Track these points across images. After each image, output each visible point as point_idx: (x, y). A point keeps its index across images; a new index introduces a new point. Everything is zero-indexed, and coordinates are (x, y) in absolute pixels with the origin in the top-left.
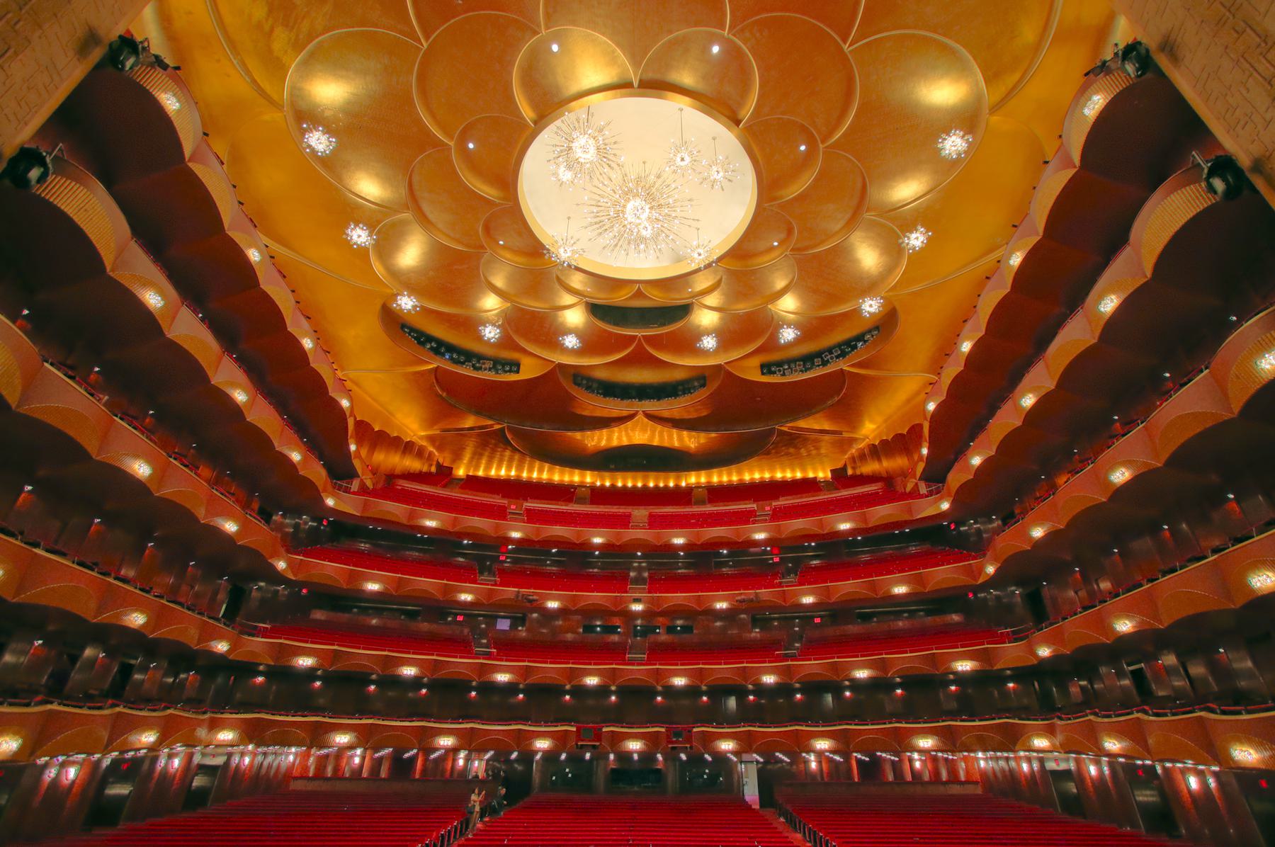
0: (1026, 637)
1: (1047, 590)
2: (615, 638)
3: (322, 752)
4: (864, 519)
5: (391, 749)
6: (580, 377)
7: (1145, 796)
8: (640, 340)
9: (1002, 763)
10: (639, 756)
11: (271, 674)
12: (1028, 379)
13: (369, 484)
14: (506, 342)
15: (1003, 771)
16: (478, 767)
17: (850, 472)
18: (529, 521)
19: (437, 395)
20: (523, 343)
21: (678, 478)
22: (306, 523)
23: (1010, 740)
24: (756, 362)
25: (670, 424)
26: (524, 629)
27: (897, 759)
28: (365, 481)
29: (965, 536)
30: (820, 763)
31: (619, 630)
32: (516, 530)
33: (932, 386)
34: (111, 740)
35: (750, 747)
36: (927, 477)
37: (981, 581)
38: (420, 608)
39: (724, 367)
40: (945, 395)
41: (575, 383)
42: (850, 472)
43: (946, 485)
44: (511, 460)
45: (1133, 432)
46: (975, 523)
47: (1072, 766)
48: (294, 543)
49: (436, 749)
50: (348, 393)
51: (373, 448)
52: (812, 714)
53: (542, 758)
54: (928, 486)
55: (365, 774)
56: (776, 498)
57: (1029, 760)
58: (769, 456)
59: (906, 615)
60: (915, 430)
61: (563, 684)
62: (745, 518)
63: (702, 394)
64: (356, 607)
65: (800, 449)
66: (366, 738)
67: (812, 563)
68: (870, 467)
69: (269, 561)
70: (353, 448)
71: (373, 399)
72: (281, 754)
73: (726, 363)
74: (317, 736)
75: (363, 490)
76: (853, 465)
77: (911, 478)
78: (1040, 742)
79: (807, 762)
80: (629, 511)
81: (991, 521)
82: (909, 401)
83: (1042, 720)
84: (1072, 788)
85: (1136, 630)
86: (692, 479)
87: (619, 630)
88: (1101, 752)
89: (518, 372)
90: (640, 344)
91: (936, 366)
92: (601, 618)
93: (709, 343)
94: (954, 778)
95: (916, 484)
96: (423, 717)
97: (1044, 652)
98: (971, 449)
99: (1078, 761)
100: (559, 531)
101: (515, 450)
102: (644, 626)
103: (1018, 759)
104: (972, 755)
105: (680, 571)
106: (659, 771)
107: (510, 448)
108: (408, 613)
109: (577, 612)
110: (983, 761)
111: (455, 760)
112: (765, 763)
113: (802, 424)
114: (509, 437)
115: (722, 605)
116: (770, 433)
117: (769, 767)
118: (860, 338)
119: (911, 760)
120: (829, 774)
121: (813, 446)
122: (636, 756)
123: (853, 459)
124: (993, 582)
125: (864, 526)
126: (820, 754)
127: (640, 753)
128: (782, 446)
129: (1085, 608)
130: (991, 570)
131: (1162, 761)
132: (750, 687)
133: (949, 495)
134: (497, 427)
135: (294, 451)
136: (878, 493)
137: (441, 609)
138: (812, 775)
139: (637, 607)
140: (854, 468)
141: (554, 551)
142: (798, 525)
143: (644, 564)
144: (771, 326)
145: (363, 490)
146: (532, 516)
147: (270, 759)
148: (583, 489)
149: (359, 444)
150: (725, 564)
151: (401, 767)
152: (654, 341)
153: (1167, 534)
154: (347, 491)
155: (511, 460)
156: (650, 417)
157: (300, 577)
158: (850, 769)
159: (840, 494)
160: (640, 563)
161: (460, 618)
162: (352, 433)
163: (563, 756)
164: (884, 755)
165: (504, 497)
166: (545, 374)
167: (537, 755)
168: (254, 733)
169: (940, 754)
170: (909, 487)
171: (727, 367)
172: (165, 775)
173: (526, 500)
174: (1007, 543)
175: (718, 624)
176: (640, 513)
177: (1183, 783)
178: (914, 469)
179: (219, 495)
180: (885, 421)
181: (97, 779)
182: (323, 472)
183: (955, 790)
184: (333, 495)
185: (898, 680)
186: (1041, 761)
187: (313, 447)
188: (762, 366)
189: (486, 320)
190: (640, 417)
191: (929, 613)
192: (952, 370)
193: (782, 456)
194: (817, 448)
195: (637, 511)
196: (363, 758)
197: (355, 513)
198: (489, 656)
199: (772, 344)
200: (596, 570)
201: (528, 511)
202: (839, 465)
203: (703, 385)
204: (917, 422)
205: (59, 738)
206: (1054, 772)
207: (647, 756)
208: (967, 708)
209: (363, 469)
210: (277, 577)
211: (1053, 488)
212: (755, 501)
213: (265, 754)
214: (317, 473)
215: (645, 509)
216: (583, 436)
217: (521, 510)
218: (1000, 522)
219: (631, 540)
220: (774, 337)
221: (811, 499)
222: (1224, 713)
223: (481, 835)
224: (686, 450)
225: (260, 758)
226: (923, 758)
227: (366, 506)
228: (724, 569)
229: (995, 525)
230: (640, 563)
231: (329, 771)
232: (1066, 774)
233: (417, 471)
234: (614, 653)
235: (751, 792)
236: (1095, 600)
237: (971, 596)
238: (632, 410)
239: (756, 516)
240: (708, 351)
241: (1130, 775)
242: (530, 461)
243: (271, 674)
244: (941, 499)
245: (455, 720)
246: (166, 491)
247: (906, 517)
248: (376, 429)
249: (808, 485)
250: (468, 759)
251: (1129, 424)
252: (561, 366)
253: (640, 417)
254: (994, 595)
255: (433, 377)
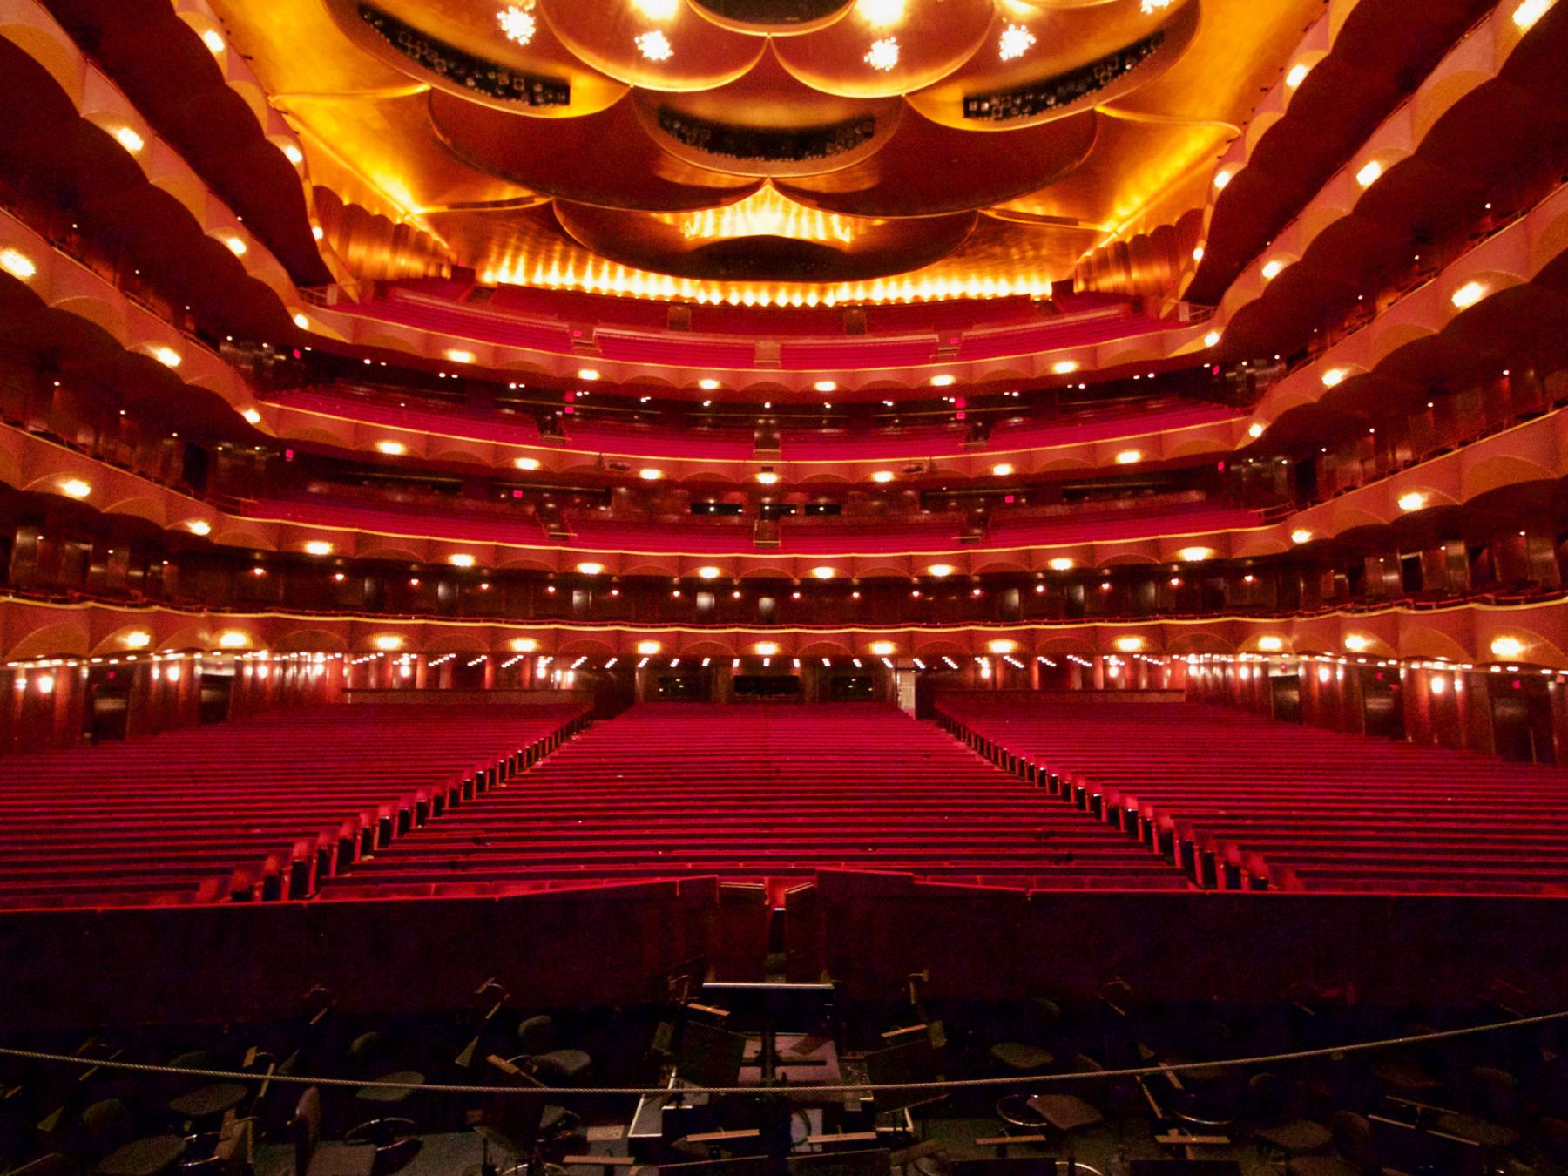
0: (1284, 519)
1: (1328, 459)
2: (736, 520)
3: (360, 661)
4: (1094, 355)
5: (453, 656)
6: (666, 110)
7: (1376, 704)
8: (769, 44)
9: (1217, 671)
10: (771, 663)
11: (270, 561)
12: (1380, 137)
13: (352, 293)
14: (544, 44)
15: (1215, 679)
16: (566, 678)
17: (1079, 287)
18: (606, 354)
19: (437, 142)
20: (573, 48)
21: (822, 292)
22: (270, 357)
23: (1234, 640)
24: (955, 94)
25: (814, 202)
26: (610, 508)
27: (1089, 665)
28: (346, 289)
29: (1233, 384)
30: (994, 669)
31: (740, 511)
32: (589, 366)
33: (1230, 144)
34: (92, 646)
35: (912, 649)
36: (1193, 296)
37: (1241, 445)
38: (459, 481)
39: (907, 103)
40: (1247, 159)
41: (662, 125)
42: (1079, 287)
43: (1219, 308)
44: (564, 260)
45: (1504, 230)
46: (1248, 367)
47: (1301, 672)
48: (264, 385)
49: (512, 654)
50: (294, 136)
51: (346, 238)
52: (993, 612)
53: (648, 665)
54: (1192, 310)
55: (419, 684)
56: (969, 326)
57: (1251, 665)
58: (962, 259)
59: (1129, 493)
60: (1193, 217)
61: (669, 575)
62: (923, 353)
63: (867, 150)
64: (368, 478)
65: (1010, 247)
66: (422, 643)
67: (1010, 421)
68: (1114, 280)
69: (236, 409)
70: (318, 233)
71: (331, 147)
72: (306, 663)
73: (909, 95)
74: (355, 641)
75: (345, 303)
76: (1086, 276)
77: (1171, 297)
78: (1270, 643)
79: (978, 668)
80: (752, 342)
81: (1272, 363)
82: (1189, 169)
83: (1279, 618)
84: (1294, 695)
85: (1427, 506)
86: (841, 294)
87: (740, 511)
88: (1340, 650)
89: (567, 102)
90: (769, 56)
91: (1241, 113)
92: (714, 497)
93: (884, 55)
94: (1155, 686)
95: (1176, 308)
96: (489, 616)
97: (1301, 537)
98: (1268, 251)
99: (1308, 666)
100: (652, 369)
101: (569, 241)
102: (776, 505)
103: (1236, 666)
104: (1183, 659)
105: (824, 431)
106: (796, 678)
107: (562, 239)
108: (443, 488)
109: (684, 485)
110: (1195, 667)
111: (533, 669)
112: (928, 670)
113: (1018, 206)
114: (560, 217)
115: (883, 477)
116: (967, 220)
117: (932, 676)
118: (1133, 53)
119: (1106, 666)
120: (1005, 684)
121: (1031, 244)
122: (767, 663)
123: (1088, 265)
124: (1257, 448)
125: (1089, 367)
126: (995, 659)
127: (774, 658)
128: (983, 243)
129: (1368, 481)
130: (1256, 431)
131: (1409, 659)
132: (915, 580)
133: (1221, 323)
134: (540, 201)
135: (232, 235)
136: (1119, 319)
137: (498, 479)
138: (981, 684)
139: (767, 479)
140: (1087, 281)
141: (643, 400)
142: (997, 364)
143: (772, 422)
144: (987, 26)
145: (345, 303)
146: (610, 348)
147: (292, 671)
148: (679, 308)
149: (325, 226)
150: (888, 422)
151: (465, 676)
152: (797, 51)
153: (1506, 384)
154: (322, 303)
155: (564, 260)
156: (784, 189)
157: (283, 434)
158: (1030, 677)
159: (1061, 321)
160: (767, 419)
161: (518, 494)
162: (438, 205)
163: (675, 663)
164: (1075, 659)
165: (560, 319)
166: (610, 109)
167: (640, 661)
168: (274, 637)
169: (1144, 658)
170: (1165, 311)
171: (911, 102)
172: (164, 683)
173: (595, 323)
174: (1288, 394)
175: (876, 503)
176: (767, 346)
177: (1425, 686)
178: (1175, 283)
179: (139, 306)
180: (1147, 203)
181: (82, 694)
182: (283, 273)
183: (1155, 698)
184: (306, 311)
185: (1107, 572)
186: (1265, 667)
187: (256, 229)
188: (967, 102)
189: (646, 24)
190: (768, 190)
191: (1159, 490)
192: (1266, 120)
193: (982, 258)
194: (1036, 247)
195: (762, 343)
196: (414, 665)
197: (342, 339)
198: (566, 541)
199: (987, 61)
200: (705, 429)
201: (603, 340)
202: (1065, 277)
203: (869, 135)
204: (1195, 207)
205: (30, 635)
206: (1276, 679)
207: (781, 661)
208: (1185, 604)
209: (340, 272)
210: (250, 435)
211: (1370, 313)
212: (936, 330)
213: (285, 665)
214: (274, 275)
215: (776, 340)
216: (677, 220)
217: (591, 340)
218: (1284, 366)
219: (756, 385)
220: (992, 47)
221: (1019, 327)
222: (1499, 603)
223: (564, 758)
224: (837, 247)
225: (278, 671)
226: (1122, 664)
227: (357, 327)
228: (887, 429)
229: (1277, 369)
230: (767, 419)
231: (373, 681)
232: (1292, 682)
233: (421, 276)
234: (741, 537)
235: (907, 697)
236: (1388, 469)
237: (1221, 466)
238: (753, 177)
239: (937, 352)
240: (883, 70)
241: (1367, 677)
242: (594, 261)
243: (270, 561)
244: (1207, 330)
245: (538, 619)
246: (61, 301)
247: (1154, 355)
248: (346, 202)
249: (1017, 306)
250: (551, 668)
251: (1504, 215)
252: (639, 94)
253: (768, 190)
254: (1254, 468)
255: (425, 107)
